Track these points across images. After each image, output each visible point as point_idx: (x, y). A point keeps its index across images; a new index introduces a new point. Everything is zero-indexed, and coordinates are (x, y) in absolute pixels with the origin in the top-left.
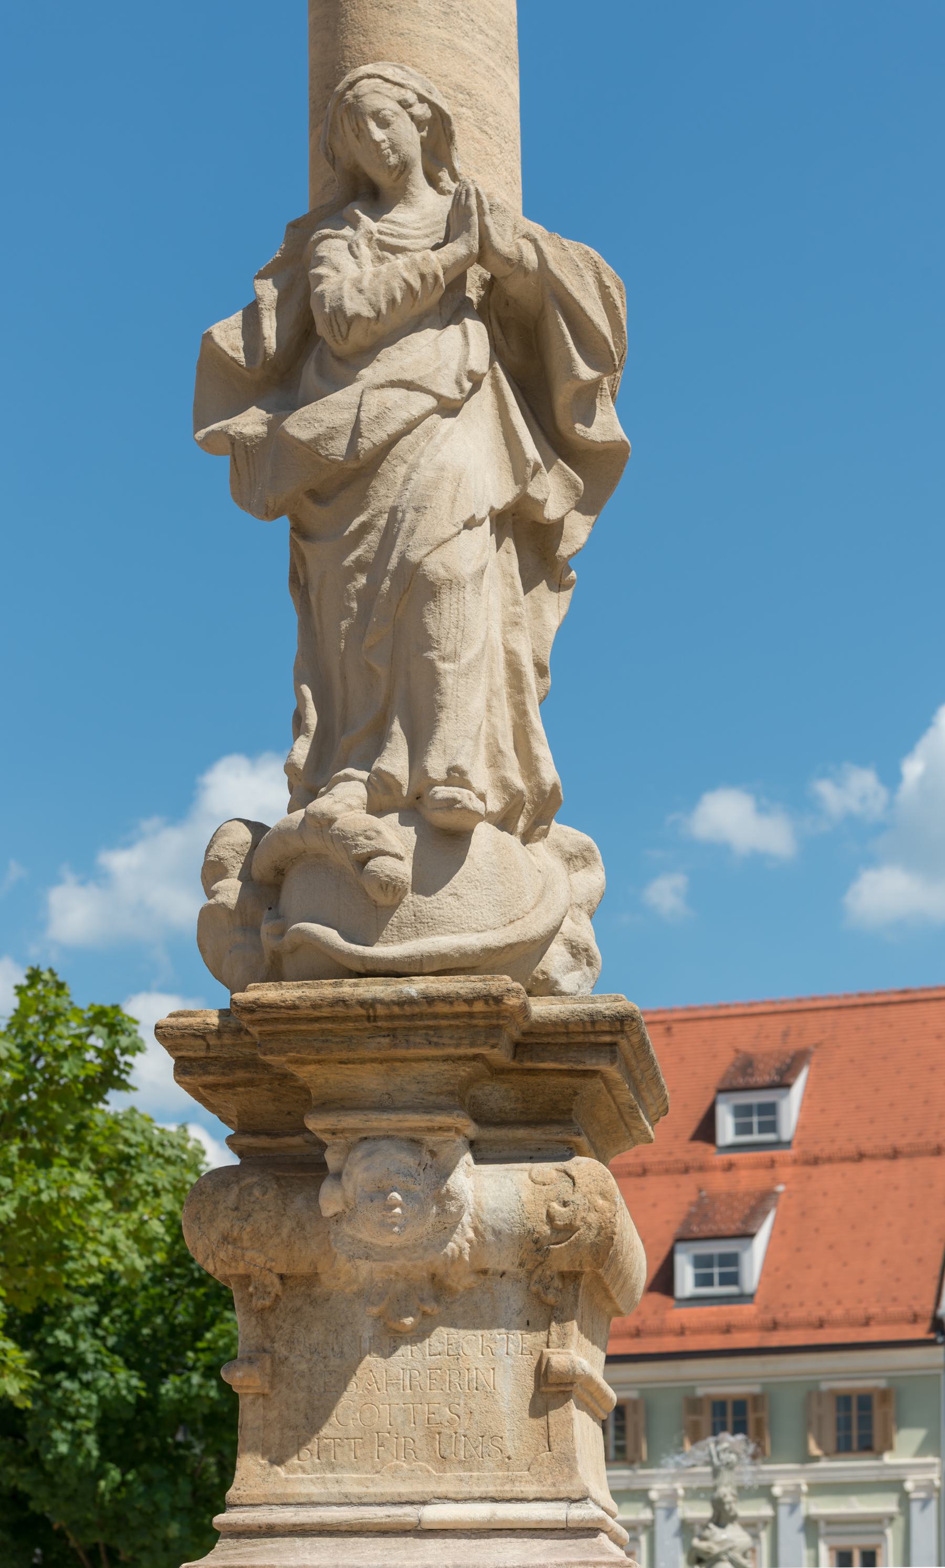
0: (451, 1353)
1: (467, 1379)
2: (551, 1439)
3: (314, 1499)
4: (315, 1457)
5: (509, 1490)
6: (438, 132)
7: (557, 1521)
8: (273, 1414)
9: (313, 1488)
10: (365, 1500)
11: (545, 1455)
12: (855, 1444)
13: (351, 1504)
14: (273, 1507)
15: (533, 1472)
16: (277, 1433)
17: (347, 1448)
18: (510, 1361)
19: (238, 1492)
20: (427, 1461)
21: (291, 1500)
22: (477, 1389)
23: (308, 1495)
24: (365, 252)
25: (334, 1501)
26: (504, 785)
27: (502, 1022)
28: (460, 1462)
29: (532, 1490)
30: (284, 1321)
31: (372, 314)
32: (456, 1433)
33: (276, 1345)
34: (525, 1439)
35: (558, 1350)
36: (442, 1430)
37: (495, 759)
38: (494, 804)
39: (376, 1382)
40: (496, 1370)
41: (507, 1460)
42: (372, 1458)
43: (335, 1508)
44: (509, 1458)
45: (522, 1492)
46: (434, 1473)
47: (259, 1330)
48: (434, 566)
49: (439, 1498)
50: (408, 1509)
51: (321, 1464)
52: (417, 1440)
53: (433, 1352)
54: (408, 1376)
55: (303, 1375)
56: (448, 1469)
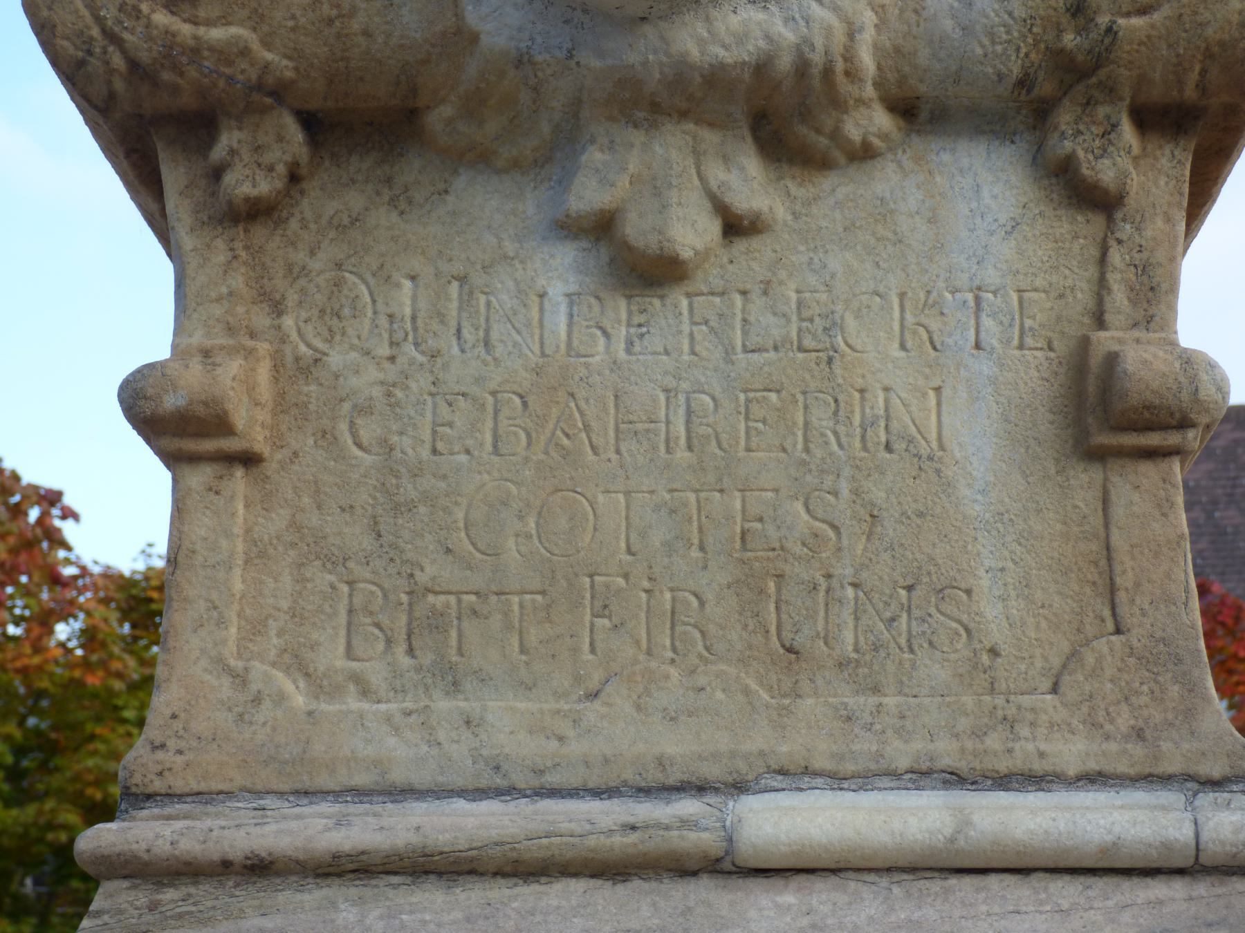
0: (808, 342)
1: (857, 420)
2: (1122, 596)
3: (398, 776)
4: (400, 650)
5: (997, 750)
7: (1167, 846)
8: (279, 520)
9: (392, 741)
10: (552, 779)
11: (1107, 647)
13: (508, 792)
14: (267, 802)
15: (1071, 695)
16: (287, 580)
17: (496, 621)
18: (985, 367)
19: (160, 755)
20: (743, 662)
21: (324, 781)
22: (888, 448)
23: (377, 763)
25: (459, 782)
28: (841, 665)
29: (1072, 752)
30: (312, 253)
31: (51, 765)
32: (829, 576)
33: (288, 322)
34: (1039, 595)
35: (1136, 333)
36: (787, 568)
39: (587, 427)
40: (946, 392)
41: (985, 658)
42: (575, 650)
43: (461, 804)
44: (994, 652)
45: (1042, 755)
46: (765, 696)
47: (237, 281)
49: (782, 772)
50: (688, 806)
51: (419, 669)
52: (709, 596)
53: (754, 341)
54: (682, 411)
55: (364, 410)
56: (805, 686)
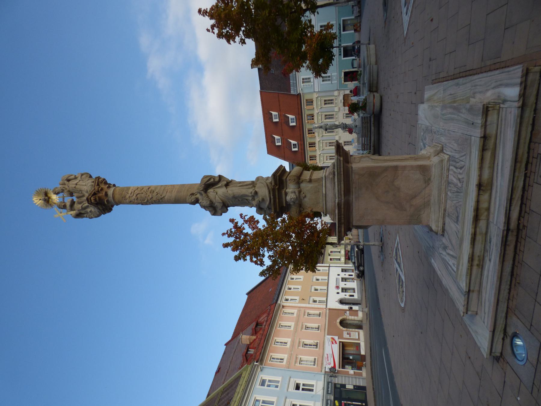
37: (249, 188)
48: (232, 195)
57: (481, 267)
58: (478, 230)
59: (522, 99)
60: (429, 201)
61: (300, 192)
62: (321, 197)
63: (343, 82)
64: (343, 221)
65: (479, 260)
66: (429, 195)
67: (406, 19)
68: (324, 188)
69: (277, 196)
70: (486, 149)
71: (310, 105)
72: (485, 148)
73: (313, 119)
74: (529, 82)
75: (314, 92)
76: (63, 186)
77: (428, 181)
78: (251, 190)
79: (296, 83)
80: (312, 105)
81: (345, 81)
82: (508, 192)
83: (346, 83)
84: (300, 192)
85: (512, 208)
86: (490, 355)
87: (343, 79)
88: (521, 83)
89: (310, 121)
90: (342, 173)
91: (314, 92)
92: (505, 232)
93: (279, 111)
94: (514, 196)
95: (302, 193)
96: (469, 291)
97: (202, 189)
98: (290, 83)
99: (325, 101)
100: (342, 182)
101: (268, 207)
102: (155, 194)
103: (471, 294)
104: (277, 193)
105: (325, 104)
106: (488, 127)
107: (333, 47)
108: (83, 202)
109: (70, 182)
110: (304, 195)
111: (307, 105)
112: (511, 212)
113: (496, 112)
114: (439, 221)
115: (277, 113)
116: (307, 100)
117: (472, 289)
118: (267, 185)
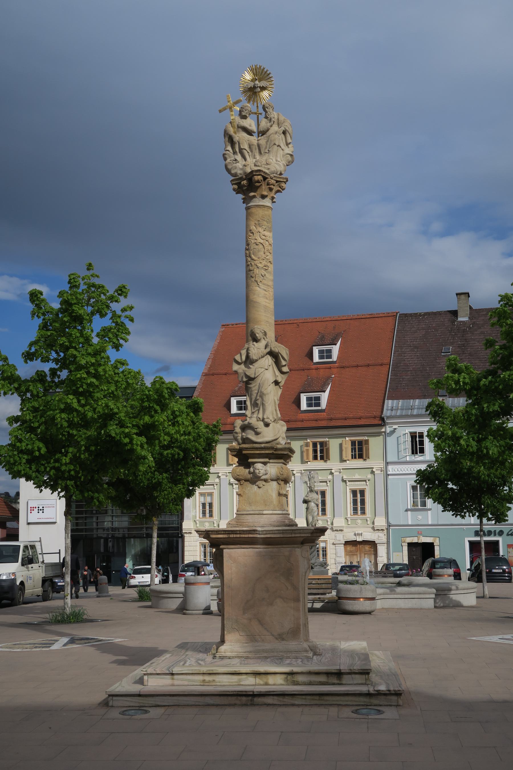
6: (265, 334)
12: (319, 458)
24: (256, 349)
26: (274, 418)
27: (265, 321)
37: (273, 414)
38: (272, 420)
48: (265, 392)
57: (202, 684)
58: (244, 677)
59: (376, 692)
60: (256, 641)
61: (266, 481)
62: (259, 508)
63: (409, 540)
64: (232, 536)
65: (209, 682)
66: (263, 641)
67: (495, 639)
68: (271, 512)
69: (263, 452)
70: (328, 677)
71: (353, 449)
72: (329, 675)
73: (315, 458)
74: (389, 697)
75: (387, 464)
76: (276, 121)
77: (281, 637)
78: (271, 418)
79: (412, 416)
80: (354, 457)
81: (410, 545)
82: (291, 691)
83: (405, 548)
84: (266, 481)
85: (275, 697)
86: (109, 695)
87: (415, 540)
88: (389, 691)
89: (311, 449)
90: (293, 535)
91: (387, 464)
92: (251, 693)
93: (342, 365)
94: (287, 697)
95: (264, 483)
96: (172, 674)
97: (273, 349)
98: (414, 398)
99: (362, 492)
100: (281, 536)
101: (248, 439)
102: (263, 272)
103: (169, 677)
104: (267, 452)
105: (354, 493)
106: (350, 676)
107: (480, 517)
108: (252, 151)
109: (282, 135)
110: (261, 486)
111: (353, 443)
112: (272, 697)
113: (364, 682)
114: (232, 652)
115: (335, 357)
116: (367, 442)
117: (176, 677)
118: (276, 439)
